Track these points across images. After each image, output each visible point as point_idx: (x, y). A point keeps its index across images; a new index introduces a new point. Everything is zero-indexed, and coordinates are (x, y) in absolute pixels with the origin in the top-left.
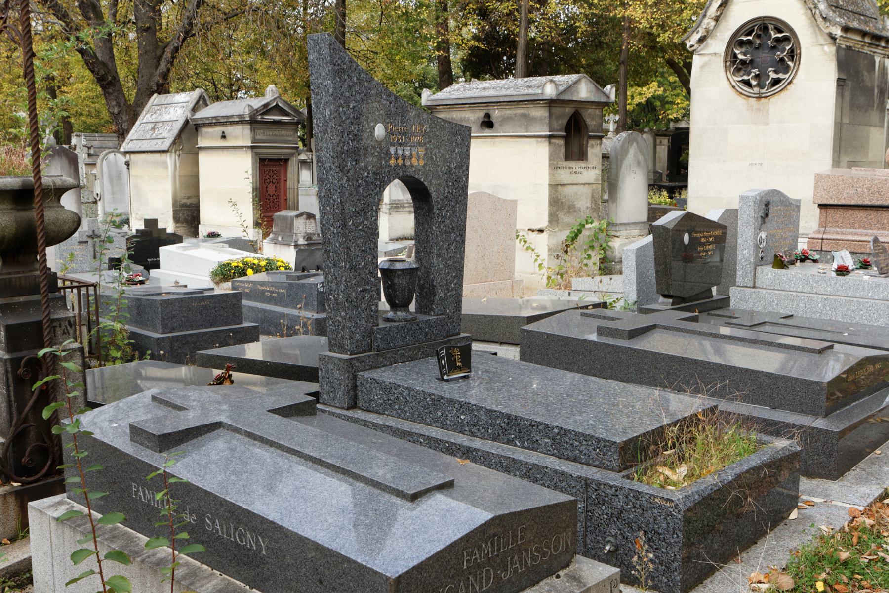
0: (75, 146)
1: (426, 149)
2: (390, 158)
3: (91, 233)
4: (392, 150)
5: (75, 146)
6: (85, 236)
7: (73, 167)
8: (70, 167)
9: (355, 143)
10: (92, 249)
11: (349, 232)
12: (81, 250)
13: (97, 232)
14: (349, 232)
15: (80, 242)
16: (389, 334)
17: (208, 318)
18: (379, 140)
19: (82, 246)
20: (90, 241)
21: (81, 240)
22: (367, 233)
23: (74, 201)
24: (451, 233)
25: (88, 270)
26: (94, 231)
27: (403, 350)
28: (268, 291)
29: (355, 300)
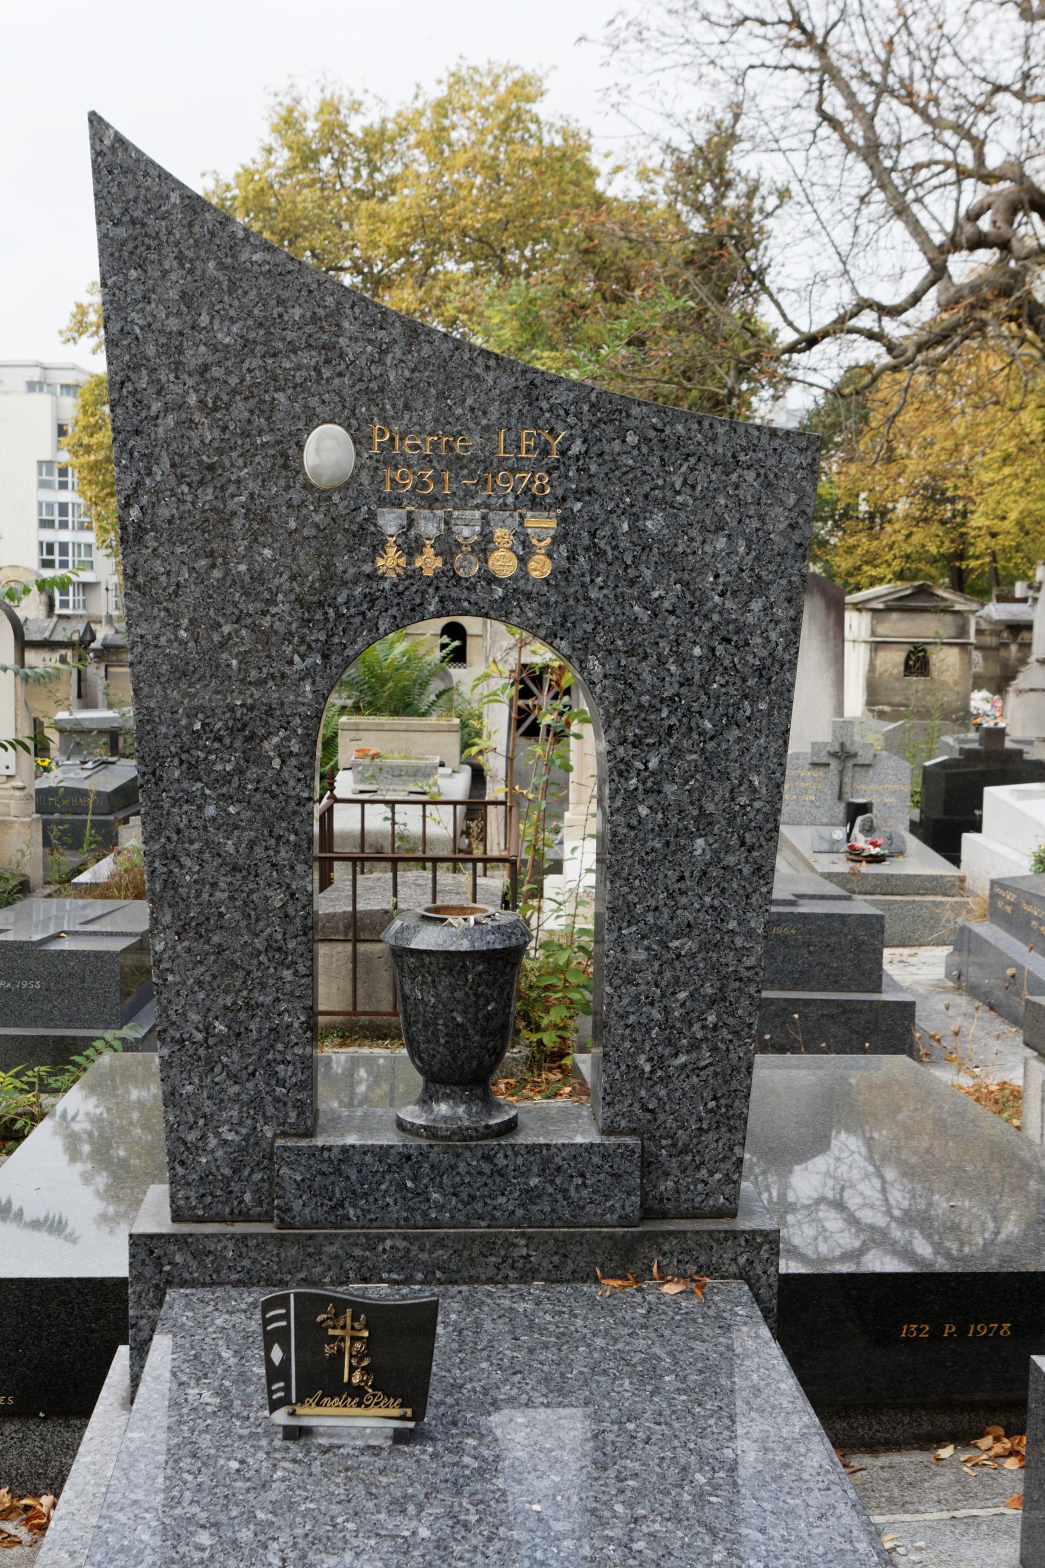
0: (1041, 583)
1: (562, 520)
2: (378, 548)
3: (837, 748)
4: (390, 521)
5: (1041, 583)
6: (824, 753)
7: (833, 615)
8: (828, 614)
9: (209, 494)
10: (837, 781)
11: (175, 802)
12: (814, 779)
13: (850, 748)
14: (175, 802)
15: (815, 765)
16: (338, 1172)
17: (789, 968)
18: (323, 481)
19: (818, 773)
20: (834, 764)
21: (816, 760)
22: (259, 809)
23: (829, 682)
24: (692, 836)
25: (825, 821)
26: (842, 744)
27: (405, 1238)
28: (1037, 918)
29: (199, 1037)
